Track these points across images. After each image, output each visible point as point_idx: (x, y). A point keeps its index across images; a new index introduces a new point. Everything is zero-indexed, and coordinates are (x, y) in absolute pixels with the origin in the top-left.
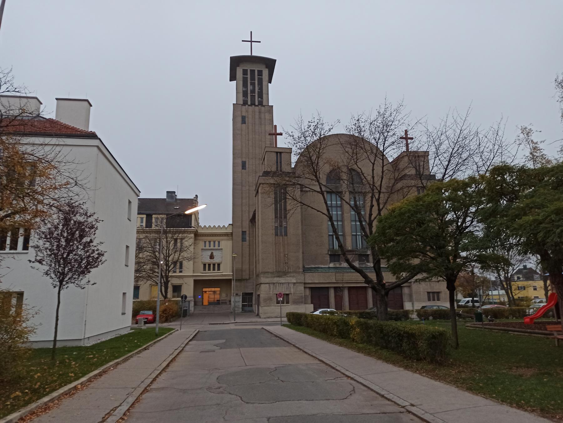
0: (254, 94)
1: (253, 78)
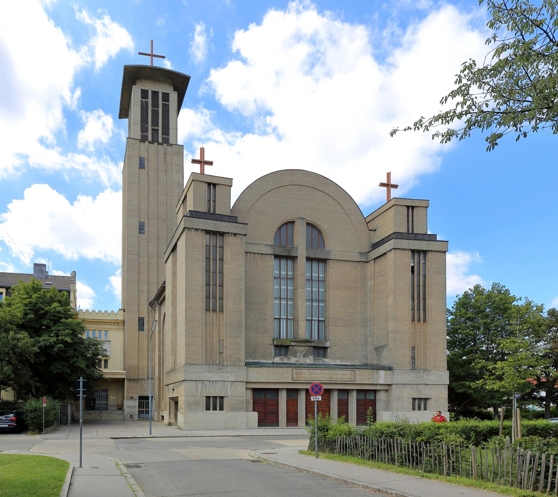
0: (156, 128)
1: (155, 104)
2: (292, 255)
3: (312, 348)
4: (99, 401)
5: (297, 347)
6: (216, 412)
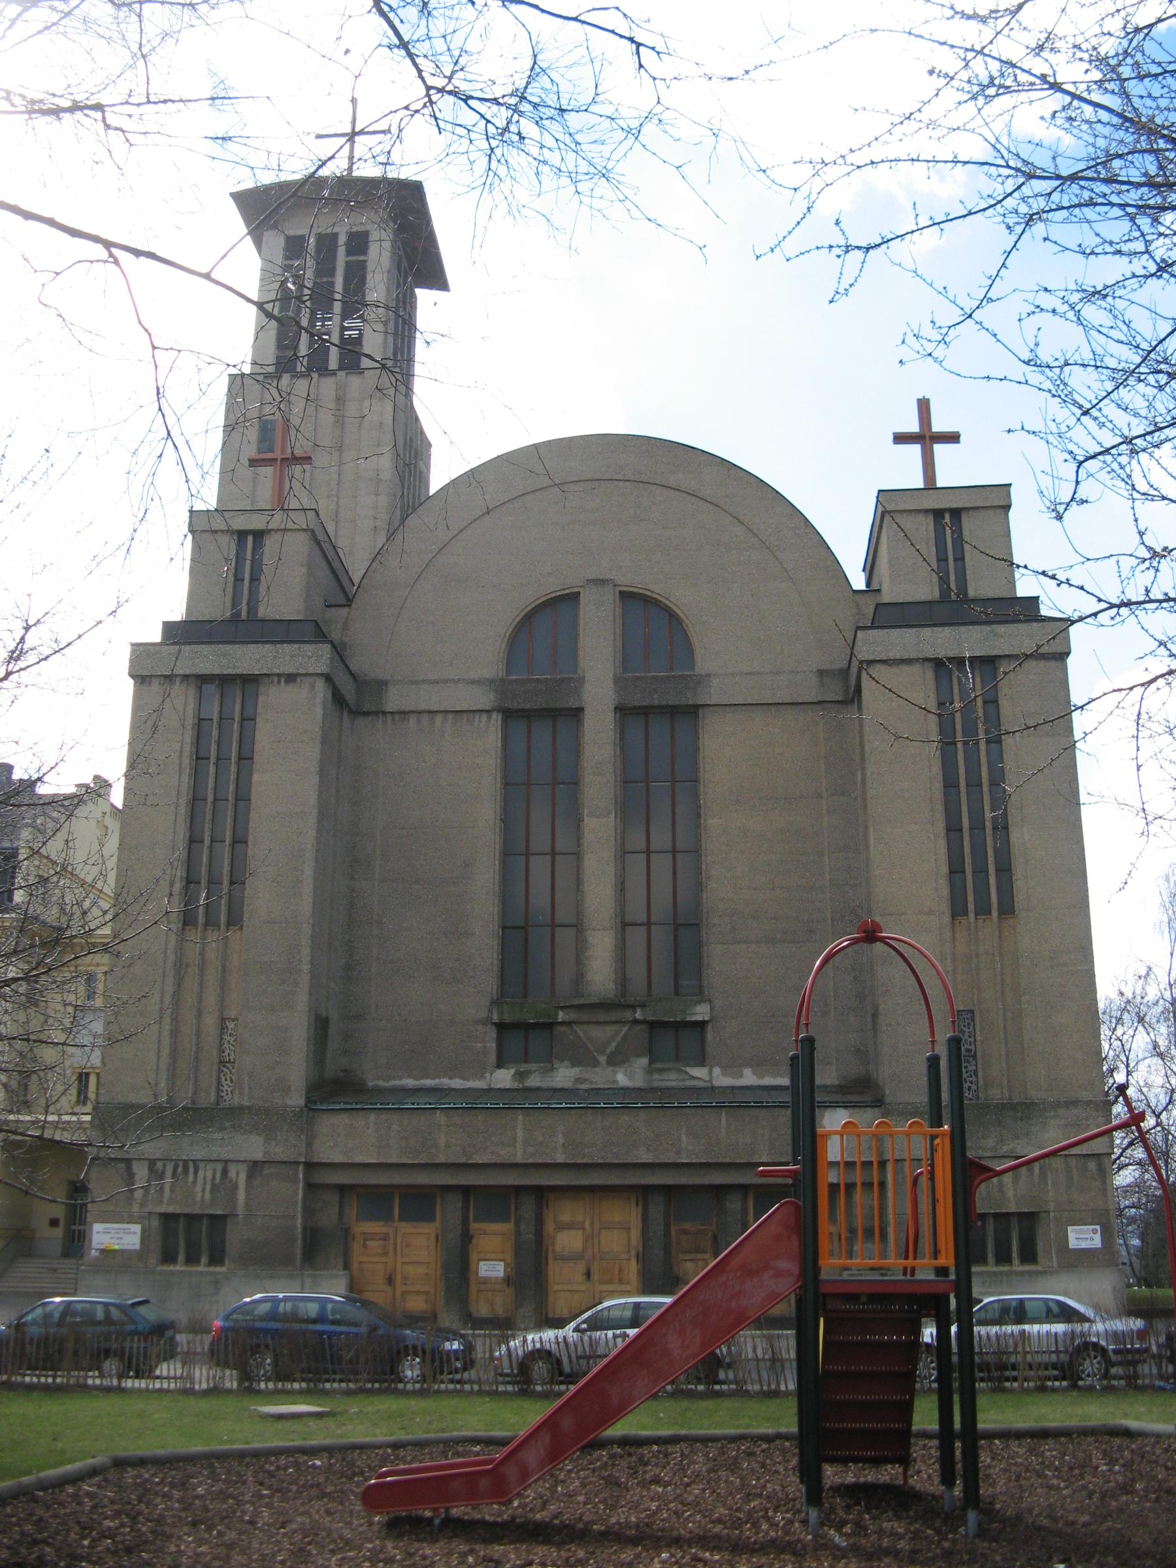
3: (643, 1027)
4: (74, 1231)
5: (585, 1027)
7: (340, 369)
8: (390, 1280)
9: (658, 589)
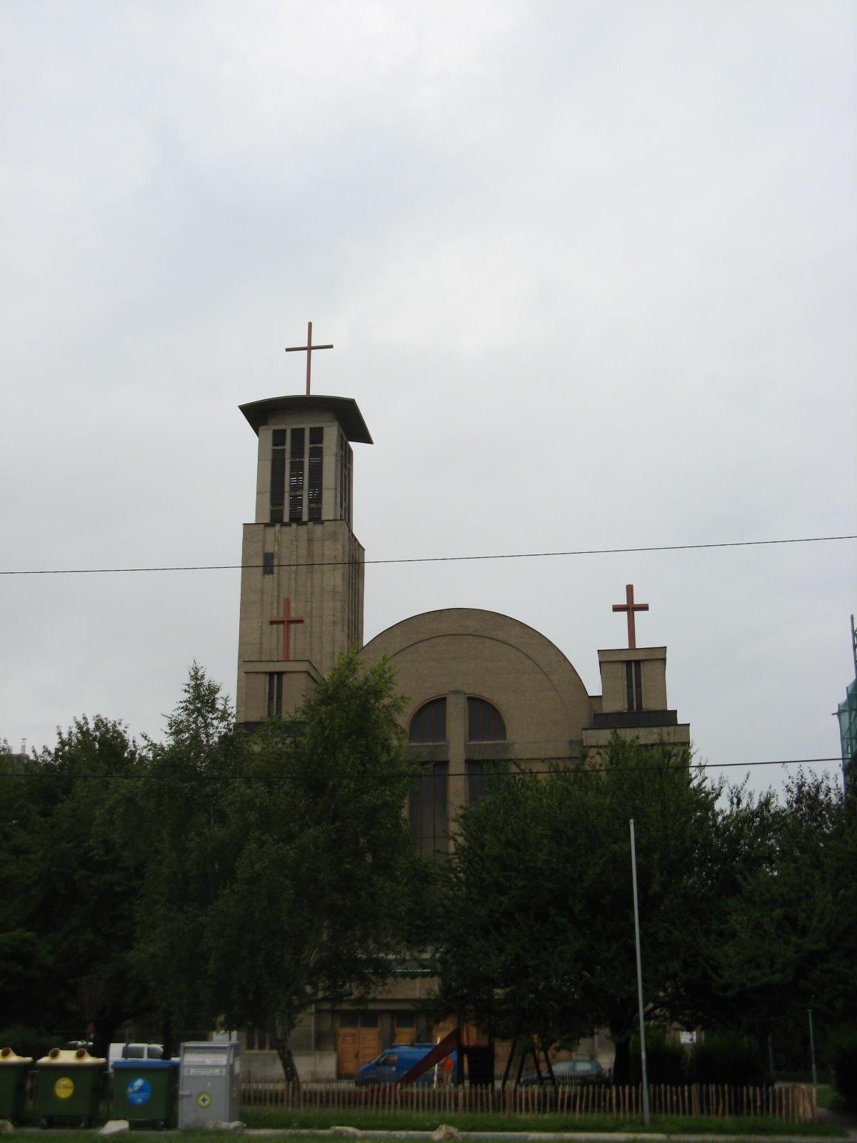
1: (297, 451)
2: (605, 712)
6: (251, 1052)
7: (310, 520)
8: (357, 1056)
9: (486, 695)
